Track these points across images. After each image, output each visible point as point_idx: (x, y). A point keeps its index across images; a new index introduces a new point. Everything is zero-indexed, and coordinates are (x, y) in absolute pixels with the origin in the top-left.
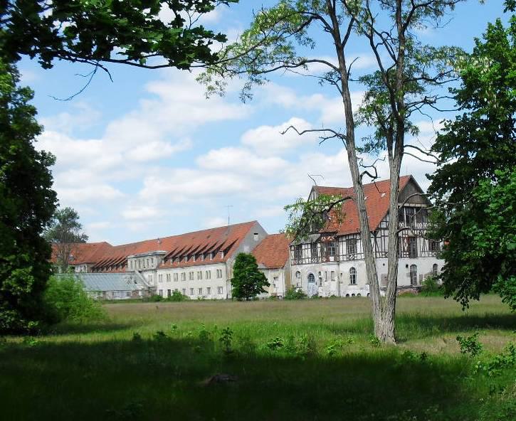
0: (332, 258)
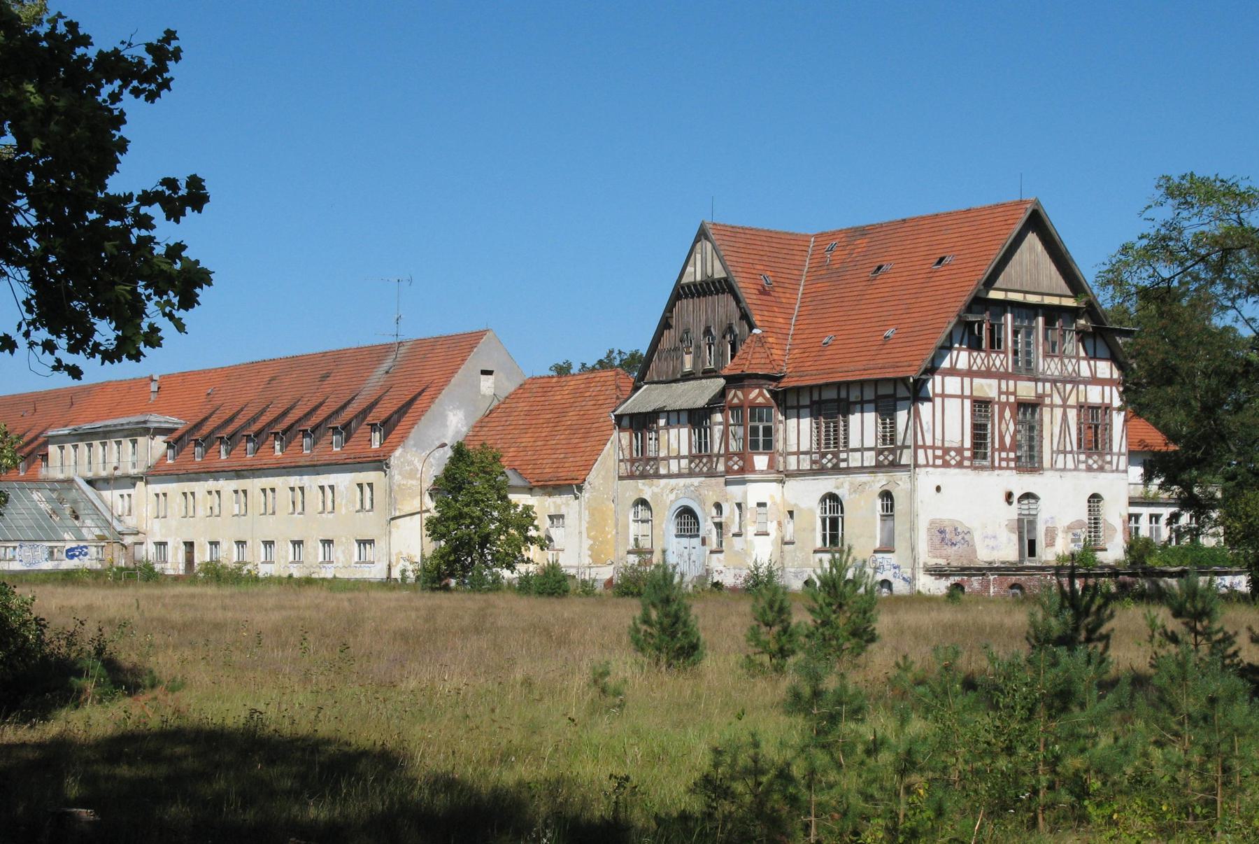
0: (761, 462)
